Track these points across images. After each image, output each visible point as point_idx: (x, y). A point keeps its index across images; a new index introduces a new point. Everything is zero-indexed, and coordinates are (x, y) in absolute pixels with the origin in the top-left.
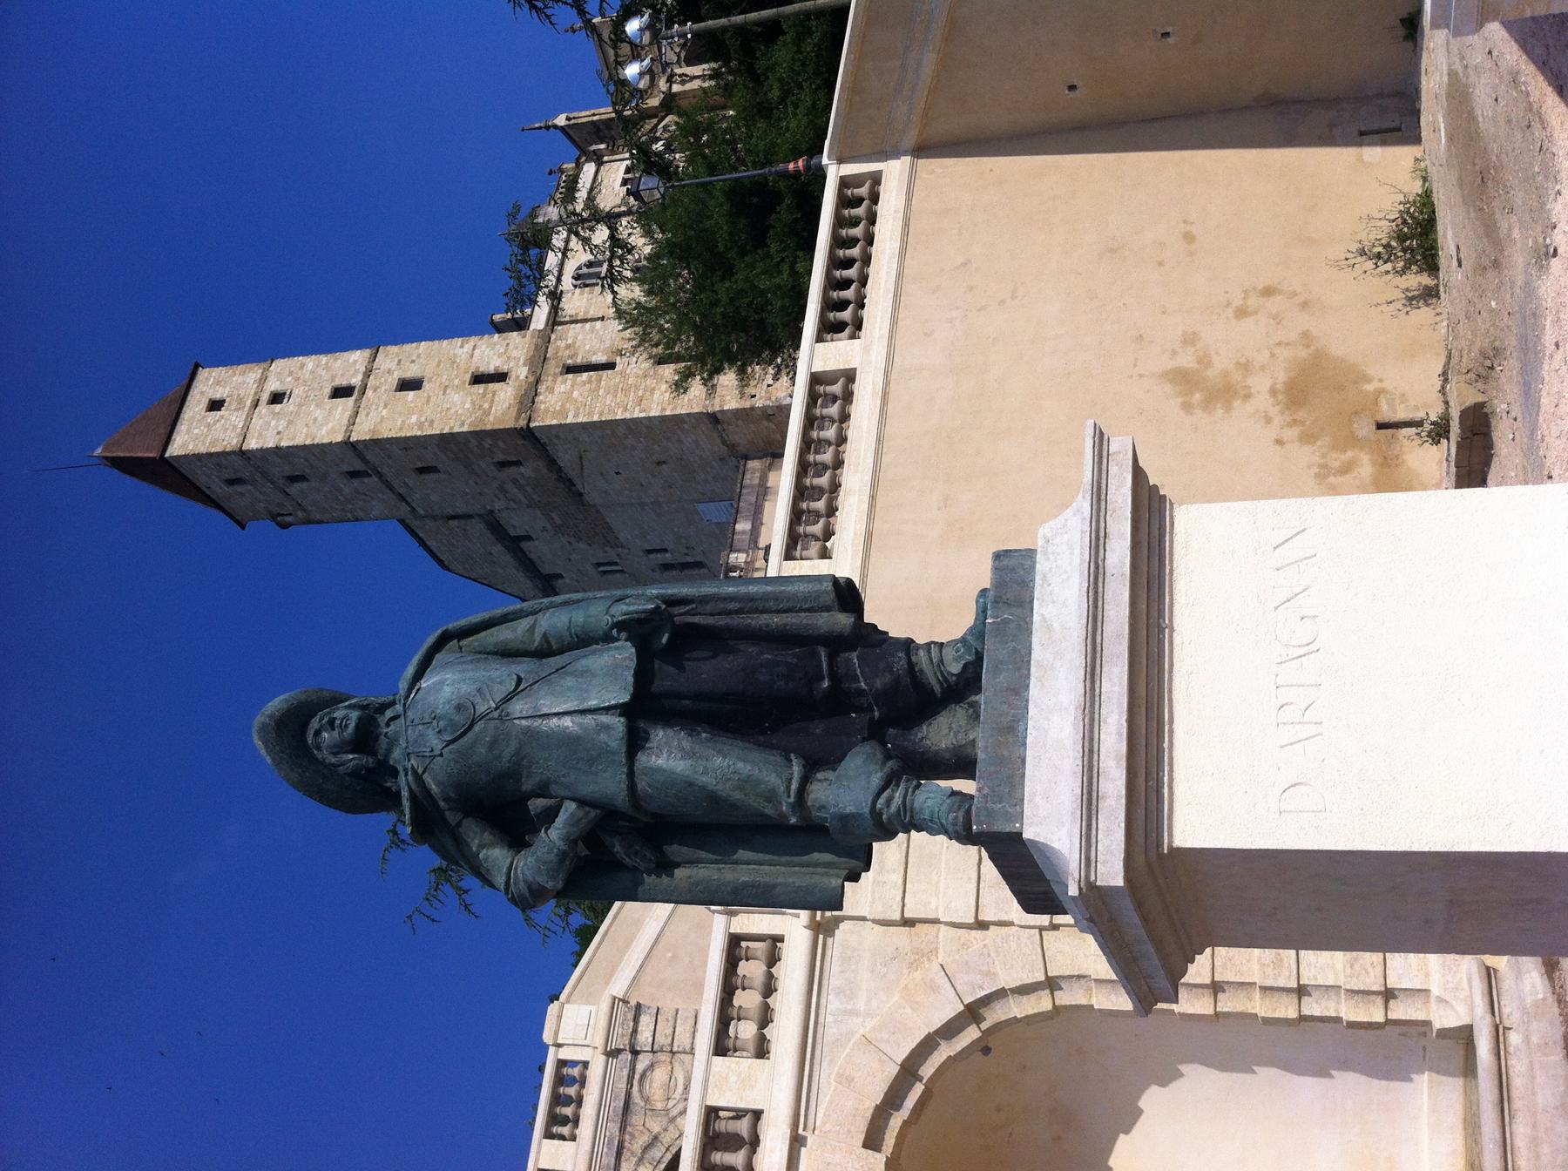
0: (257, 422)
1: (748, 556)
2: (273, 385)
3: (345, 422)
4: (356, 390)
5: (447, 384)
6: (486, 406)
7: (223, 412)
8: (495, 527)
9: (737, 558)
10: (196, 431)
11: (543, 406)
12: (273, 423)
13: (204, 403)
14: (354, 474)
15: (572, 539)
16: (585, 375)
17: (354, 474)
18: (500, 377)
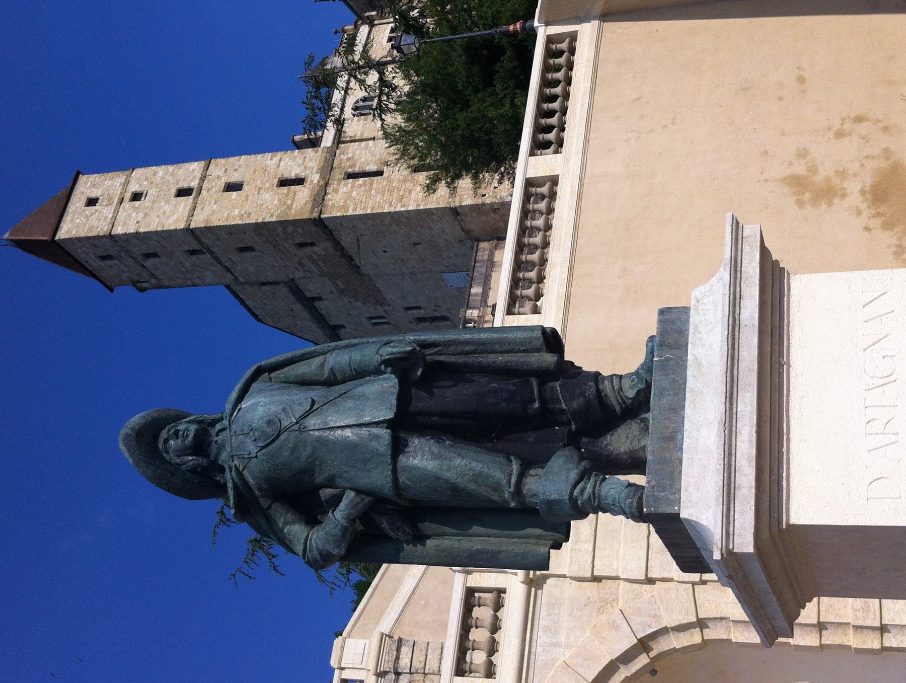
0: (122, 214)
1: (480, 311)
2: (134, 187)
3: (186, 214)
4: (195, 191)
5: (260, 187)
6: (289, 202)
7: (97, 207)
8: (296, 291)
9: (472, 313)
10: (78, 221)
11: (330, 203)
12: (134, 215)
13: (84, 201)
14: (192, 252)
15: (352, 300)
16: (361, 180)
17: (192, 252)
18: (299, 181)
